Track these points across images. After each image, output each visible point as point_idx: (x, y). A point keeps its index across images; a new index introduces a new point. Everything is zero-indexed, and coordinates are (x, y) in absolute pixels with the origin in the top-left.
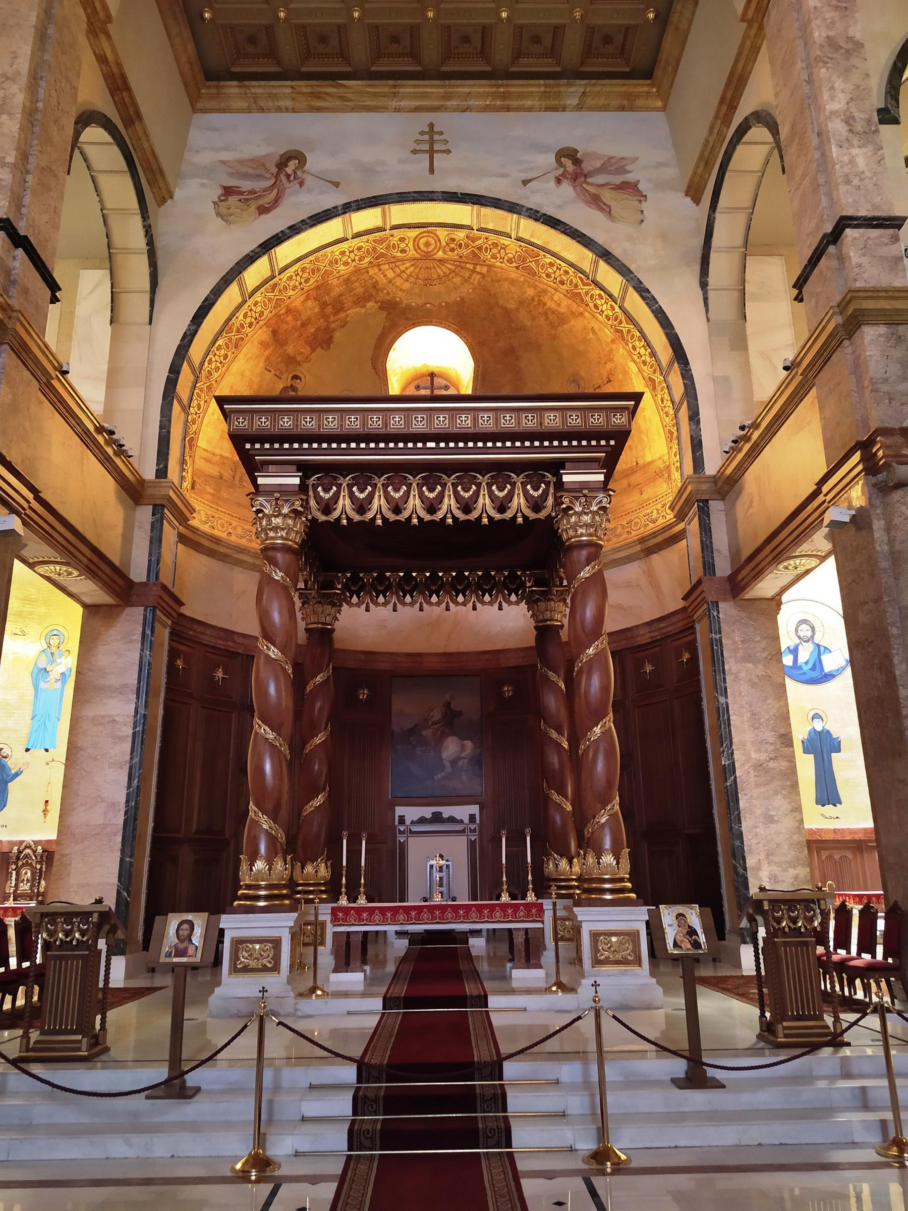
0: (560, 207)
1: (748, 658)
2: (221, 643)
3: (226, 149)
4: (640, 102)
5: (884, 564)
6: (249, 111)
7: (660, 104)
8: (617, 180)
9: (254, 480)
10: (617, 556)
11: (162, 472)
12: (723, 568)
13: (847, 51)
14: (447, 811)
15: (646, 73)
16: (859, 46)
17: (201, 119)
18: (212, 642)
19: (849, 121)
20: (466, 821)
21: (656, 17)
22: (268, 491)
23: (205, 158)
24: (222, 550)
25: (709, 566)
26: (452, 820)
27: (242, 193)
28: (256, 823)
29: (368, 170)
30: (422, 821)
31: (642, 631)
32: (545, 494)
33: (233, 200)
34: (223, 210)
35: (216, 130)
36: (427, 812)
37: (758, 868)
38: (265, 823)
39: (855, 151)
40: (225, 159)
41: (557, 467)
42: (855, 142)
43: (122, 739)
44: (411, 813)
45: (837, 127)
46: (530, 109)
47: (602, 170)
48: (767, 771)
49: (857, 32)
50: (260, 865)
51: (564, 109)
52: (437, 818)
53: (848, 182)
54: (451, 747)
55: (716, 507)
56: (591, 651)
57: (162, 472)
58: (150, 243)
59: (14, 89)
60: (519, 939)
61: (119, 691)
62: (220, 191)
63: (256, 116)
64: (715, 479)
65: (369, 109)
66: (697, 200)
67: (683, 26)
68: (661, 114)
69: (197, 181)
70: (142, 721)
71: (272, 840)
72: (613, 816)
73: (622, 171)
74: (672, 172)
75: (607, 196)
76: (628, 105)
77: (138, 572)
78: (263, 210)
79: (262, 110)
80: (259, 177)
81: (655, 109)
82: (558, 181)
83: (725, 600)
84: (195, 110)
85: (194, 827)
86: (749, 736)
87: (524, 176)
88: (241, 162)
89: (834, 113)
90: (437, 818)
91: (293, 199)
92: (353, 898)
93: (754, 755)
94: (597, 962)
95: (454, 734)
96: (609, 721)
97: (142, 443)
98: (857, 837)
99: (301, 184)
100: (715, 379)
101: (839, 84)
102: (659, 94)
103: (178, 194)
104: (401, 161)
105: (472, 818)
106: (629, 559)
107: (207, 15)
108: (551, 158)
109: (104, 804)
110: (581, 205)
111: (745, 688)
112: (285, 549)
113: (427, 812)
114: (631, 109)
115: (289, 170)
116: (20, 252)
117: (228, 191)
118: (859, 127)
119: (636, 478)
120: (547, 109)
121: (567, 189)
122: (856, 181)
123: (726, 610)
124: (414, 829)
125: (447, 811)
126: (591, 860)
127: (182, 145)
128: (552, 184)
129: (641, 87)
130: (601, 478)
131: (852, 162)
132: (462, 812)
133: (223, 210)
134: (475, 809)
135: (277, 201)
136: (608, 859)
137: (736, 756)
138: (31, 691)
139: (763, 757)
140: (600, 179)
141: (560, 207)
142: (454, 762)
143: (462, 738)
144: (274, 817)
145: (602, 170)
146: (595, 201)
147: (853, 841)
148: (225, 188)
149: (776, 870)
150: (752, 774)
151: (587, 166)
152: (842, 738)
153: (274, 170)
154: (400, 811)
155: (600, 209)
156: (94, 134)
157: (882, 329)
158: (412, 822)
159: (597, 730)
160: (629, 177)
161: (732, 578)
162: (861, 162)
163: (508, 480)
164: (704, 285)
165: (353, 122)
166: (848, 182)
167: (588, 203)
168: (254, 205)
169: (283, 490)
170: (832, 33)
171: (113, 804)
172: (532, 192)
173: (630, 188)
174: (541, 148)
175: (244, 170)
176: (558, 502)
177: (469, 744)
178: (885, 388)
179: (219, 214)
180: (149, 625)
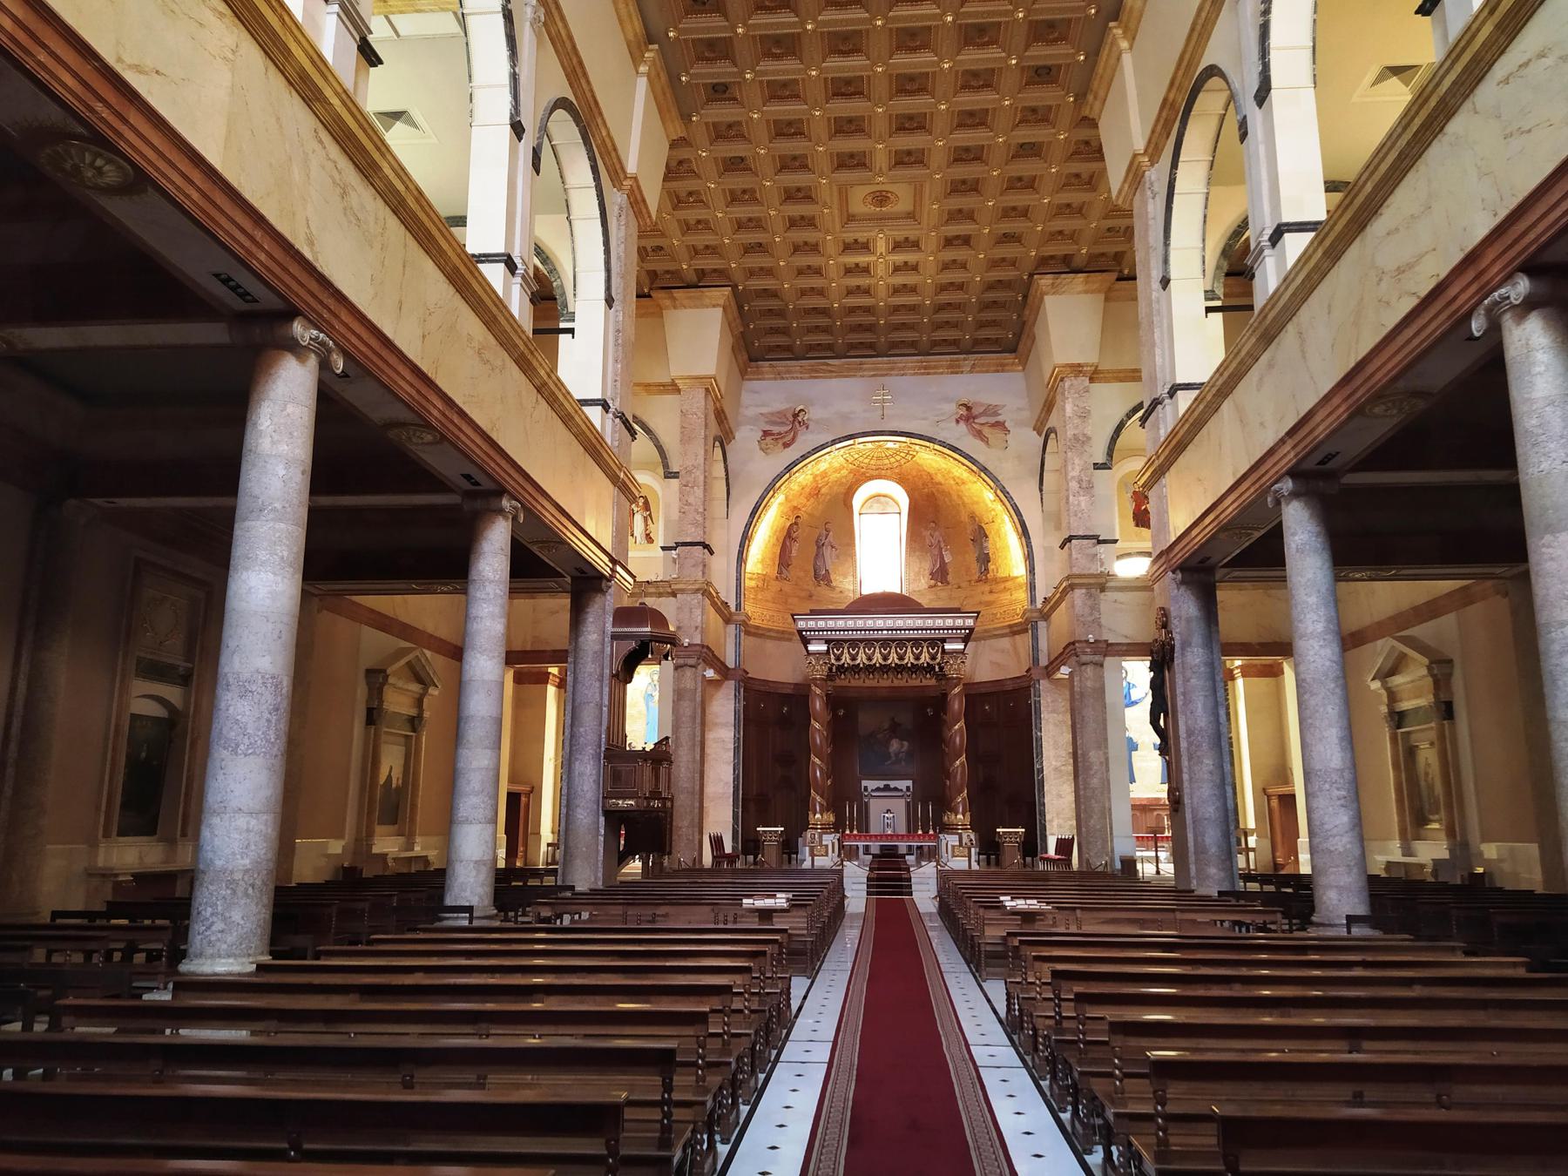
0: (958, 439)
1: (1054, 711)
2: (762, 688)
3: (763, 405)
4: (1007, 368)
5: (1077, 697)
6: (775, 379)
7: (1021, 368)
8: (992, 420)
9: (806, 648)
10: (996, 633)
11: (738, 606)
12: (1044, 662)
13: (1083, 442)
14: (893, 784)
15: (1013, 350)
16: (1089, 439)
17: (748, 385)
18: (757, 688)
19: (1080, 482)
20: (905, 790)
21: (1097, 12)
22: (814, 654)
23: (751, 412)
24: (760, 632)
25: (1036, 660)
26: (896, 789)
27: (773, 434)
28: (814, 799)
29: (845, 417)
30: (878, 789)
31: (1008, 682)
32: (938, 651)
33: (769, 439)
34: (763, 446)
35: (756, 392)
36: (881, 784)
37: (1051, 821)
38: (818, 798)
39: (1082, 498)
40: (763, 412)
41: (944, 640)
42: (1081, 493)
43: (729, 750)
44: (871, 784)
45: (1074, 485)
46: (942, 373)
47: (984, 414)
48: (1060, 771)
49: (1088, 431)
50: (818, 816)
51: (962, 372)
52: (887, 788)
53: (1076, 515)
54: (895, 745)
55: (1042, 624)
56: (956, 727)
57: (738, 606)
58: (727, 475)
59: (698, 473)
60: (926, 850)
61: (725, 725)
62: (761, 434)
63: (779, 382)
64: (1040, 611)
65: (846, 377)
66: (1040, 435)
67: (1101, 93)
68: (1021, 374)
69: (748, 427)
70: (736, 740)
71: (821, 805)
72: (964, 799)
73: (997, 414)
74: (1026, 414)
75: (986, 431)
76: (1001, 368)
77: (731, 663)
78: (786, 445)
79: (783, 378)
80: (783, 424)
81: (1019, 371)
82: (957, 422)
83: (1043, 679)
84: (743, 379)
85: (755, 793)
86: (1052, 753)
87: (937, 419)
88: (772, 414)
89: (1073, 477)
90: (887, 788)
91: (804, 438)
92: (851, 831)
93: (1054, 763)
94: (953, 856)
95: (896, 737)
96: (963, 758)
97: (728, 591)
98: (1143, 803)
99: (807, 428)
100: (1045, 548)
101: (1077, 461)
102: (1020, 363)
103: (737, 435)
104: (865, 411)
105: (908, 788)
106: (1003, 636)
107: (671, 34)
108: (953, 407)
109: (722, 783)
110: (971, 437)
111: (1051, 727)
112: (821, 679)
113: (881, 784)
114: (1003, 371)
115: (800, 419)
116: (706, 550)
117: (766, 433)
118: (1084, 485)
119: (1008, 584)
120: (952, 373)
121: (963, 426)
122: (1080, 515)
123: (1044, 685)
124: (873, 794)
125: (893, 784)
126: (953, 817)
127: (737, 403)
128: (954, 424)
129: (1008, 358)
130: (962, 647)
131: (1079, 505)
132: (903, 784)
133: (763, 446)
134: (909, 783)
135: (793, 440)
136: (960, 816)
137: (1044, 763)
138: (644, 708)
139: (1059, 764)
140: (982, 420)
141: (958, 439)
142: (897, 755)
143: (902, 739)
144: (822, 797)
145: (984, 414)
146: (979, 435)
147: (1141, 805)
148: (764, 431)
149: (1061, 821)
150: (1053, 772)
151: (975, 411)
152: (1139, 742)
153: (791, 419)
154: (864, 783)
155: (982, 440)
156: (561, 114)
157: (1084, 591)
158: (872, 790)
159: (958, 762)
160: (1000, 418)
161: (1047, 667)
162: (1083, 505)
163: (920, 645)
164: (1041, 490)
165: (835, 384)
166: (1076, 515)
167: (974, 436)
168: (781, 442)
169: (819, 653)
170: (1076, 432)
171: (727, 783)
172: (942, 429)
173: (1000, 425)
174: (947, 400)
175: (774, 419)
176: (942, 658)
177: (906, 743)
178: (1081, 619)
179: (762, 449)
180: (737, 690)
